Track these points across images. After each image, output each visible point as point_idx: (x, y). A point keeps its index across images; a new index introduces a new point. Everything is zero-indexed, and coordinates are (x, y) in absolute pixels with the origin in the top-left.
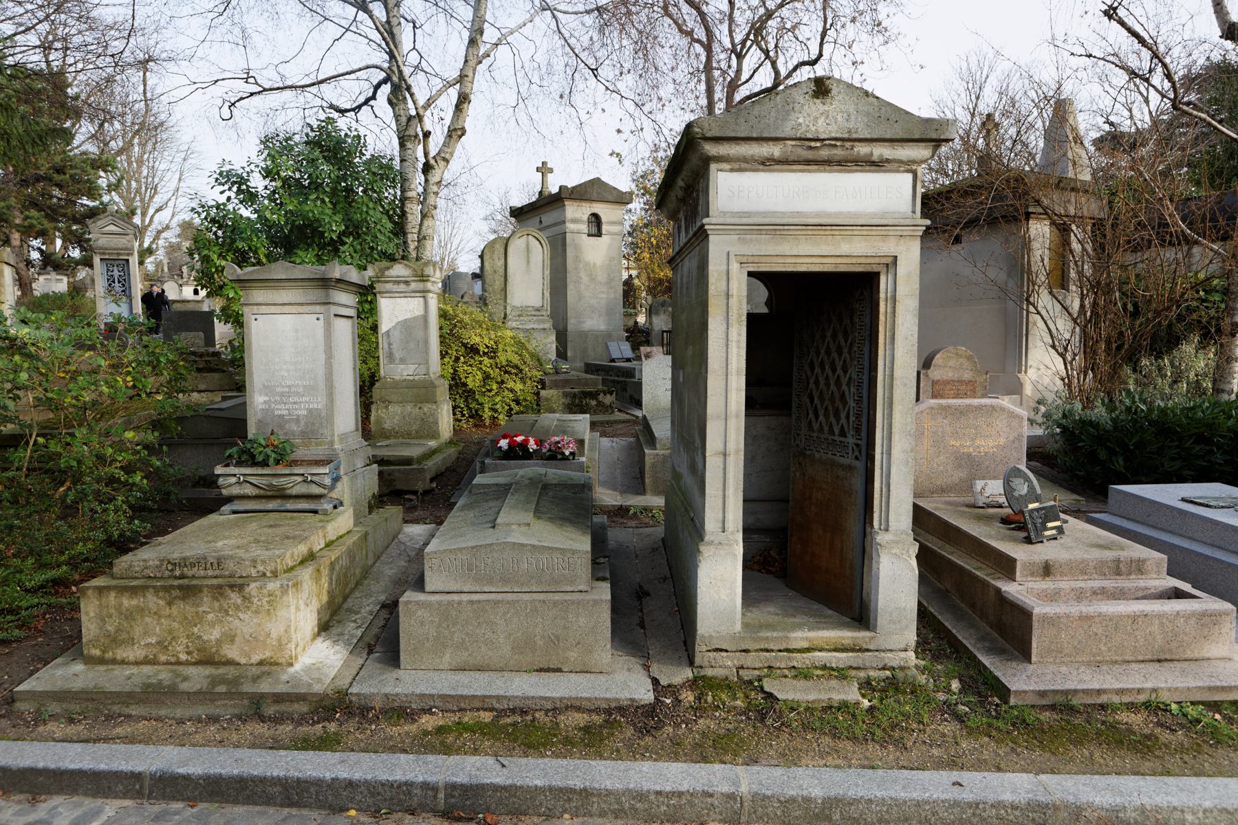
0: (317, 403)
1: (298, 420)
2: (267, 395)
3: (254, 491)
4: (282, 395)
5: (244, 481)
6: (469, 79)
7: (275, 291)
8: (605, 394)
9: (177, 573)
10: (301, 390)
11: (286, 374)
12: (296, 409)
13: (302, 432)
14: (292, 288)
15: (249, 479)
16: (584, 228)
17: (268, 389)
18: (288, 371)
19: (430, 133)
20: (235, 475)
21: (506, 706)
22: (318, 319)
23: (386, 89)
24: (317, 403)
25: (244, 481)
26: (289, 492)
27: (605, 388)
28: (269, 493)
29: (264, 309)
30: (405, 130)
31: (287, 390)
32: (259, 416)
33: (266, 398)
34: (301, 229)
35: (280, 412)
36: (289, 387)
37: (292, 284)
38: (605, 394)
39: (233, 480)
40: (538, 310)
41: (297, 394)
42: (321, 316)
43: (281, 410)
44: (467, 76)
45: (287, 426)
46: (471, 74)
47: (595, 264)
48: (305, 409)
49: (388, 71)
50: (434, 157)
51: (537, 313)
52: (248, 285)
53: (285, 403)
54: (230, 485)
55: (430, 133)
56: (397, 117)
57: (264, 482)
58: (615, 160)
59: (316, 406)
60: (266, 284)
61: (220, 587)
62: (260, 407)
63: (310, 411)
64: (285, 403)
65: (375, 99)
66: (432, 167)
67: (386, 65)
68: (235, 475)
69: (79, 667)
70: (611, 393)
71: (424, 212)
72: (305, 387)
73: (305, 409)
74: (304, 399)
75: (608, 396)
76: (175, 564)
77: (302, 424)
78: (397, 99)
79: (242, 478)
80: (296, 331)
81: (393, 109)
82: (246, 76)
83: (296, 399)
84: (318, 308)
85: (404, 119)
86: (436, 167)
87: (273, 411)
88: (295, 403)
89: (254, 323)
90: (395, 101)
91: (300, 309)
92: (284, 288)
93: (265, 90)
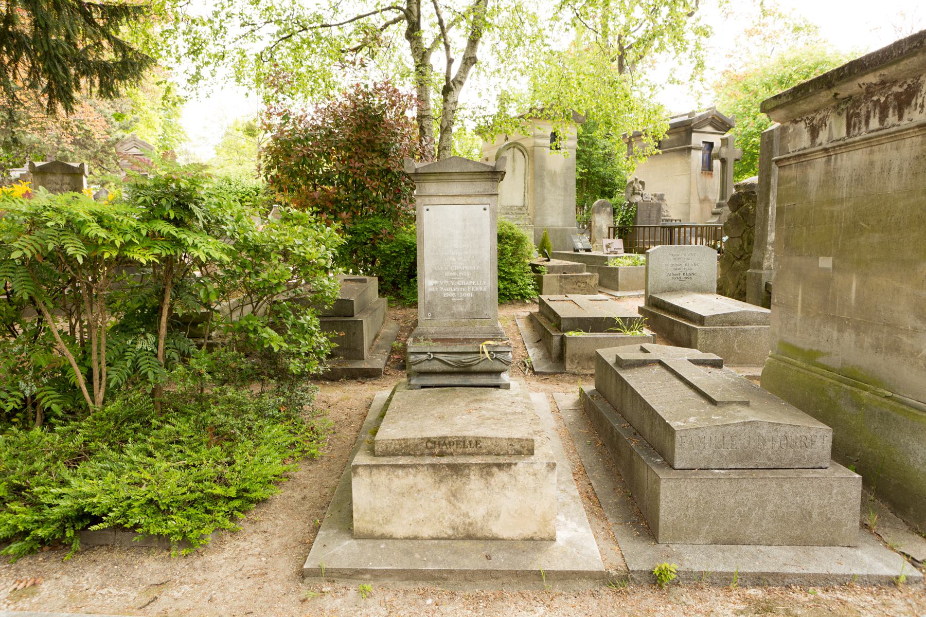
0: (483, 286)
1: (464, 301)
3: (445, 368)
4: (450, 278)
5: (434, 358)
9: (437, 451)
11: (454, 260)
12: (463, 292)
14: (463, 181)
15: (438, 356)
16: (547, 142)
17: (436, 273)
19: (453, 60)
20: (426, 353)
21: (735, 570)
22: (485, 209)
25: (434, 358)
26: (474, 368)
28: (456, 369)
29: (435, 200)
31: (455, 274)
32: (429, 298)
35: (448, 295)
36: (457, 271)
39: (424, 357)
40: (520, 209)
41: (465, 277)
42: (487, 207)
43: (449, 293)
45: (454, 308)
47: (555, 172)
48: (471, 291)
50: (453, 81)
51: (519, 211)
52: (424, 178)
53: (453, 287)
54: (421, 362)
55: (453, 60)
57: (453, 359)
58: (690, 77)
59: (481, 289)
61: (489, 465)
62: (430, 290)
63: (475, 293)
66: (451, 90)
67: (405, 7)
68: (426, 353)
69: (348, 543)
71: (444, 127)
72: (471, 271)
73: (471, 291)
74: (470, 282)
76: (435, 442)
79: (432, 356)
80: (464, 220)
83: (463, 282)
84: (485, 200)
86: (454, 89)
88: (461, 286)
89: (426, 213)
91: (470, 200)
92: (453, 181)
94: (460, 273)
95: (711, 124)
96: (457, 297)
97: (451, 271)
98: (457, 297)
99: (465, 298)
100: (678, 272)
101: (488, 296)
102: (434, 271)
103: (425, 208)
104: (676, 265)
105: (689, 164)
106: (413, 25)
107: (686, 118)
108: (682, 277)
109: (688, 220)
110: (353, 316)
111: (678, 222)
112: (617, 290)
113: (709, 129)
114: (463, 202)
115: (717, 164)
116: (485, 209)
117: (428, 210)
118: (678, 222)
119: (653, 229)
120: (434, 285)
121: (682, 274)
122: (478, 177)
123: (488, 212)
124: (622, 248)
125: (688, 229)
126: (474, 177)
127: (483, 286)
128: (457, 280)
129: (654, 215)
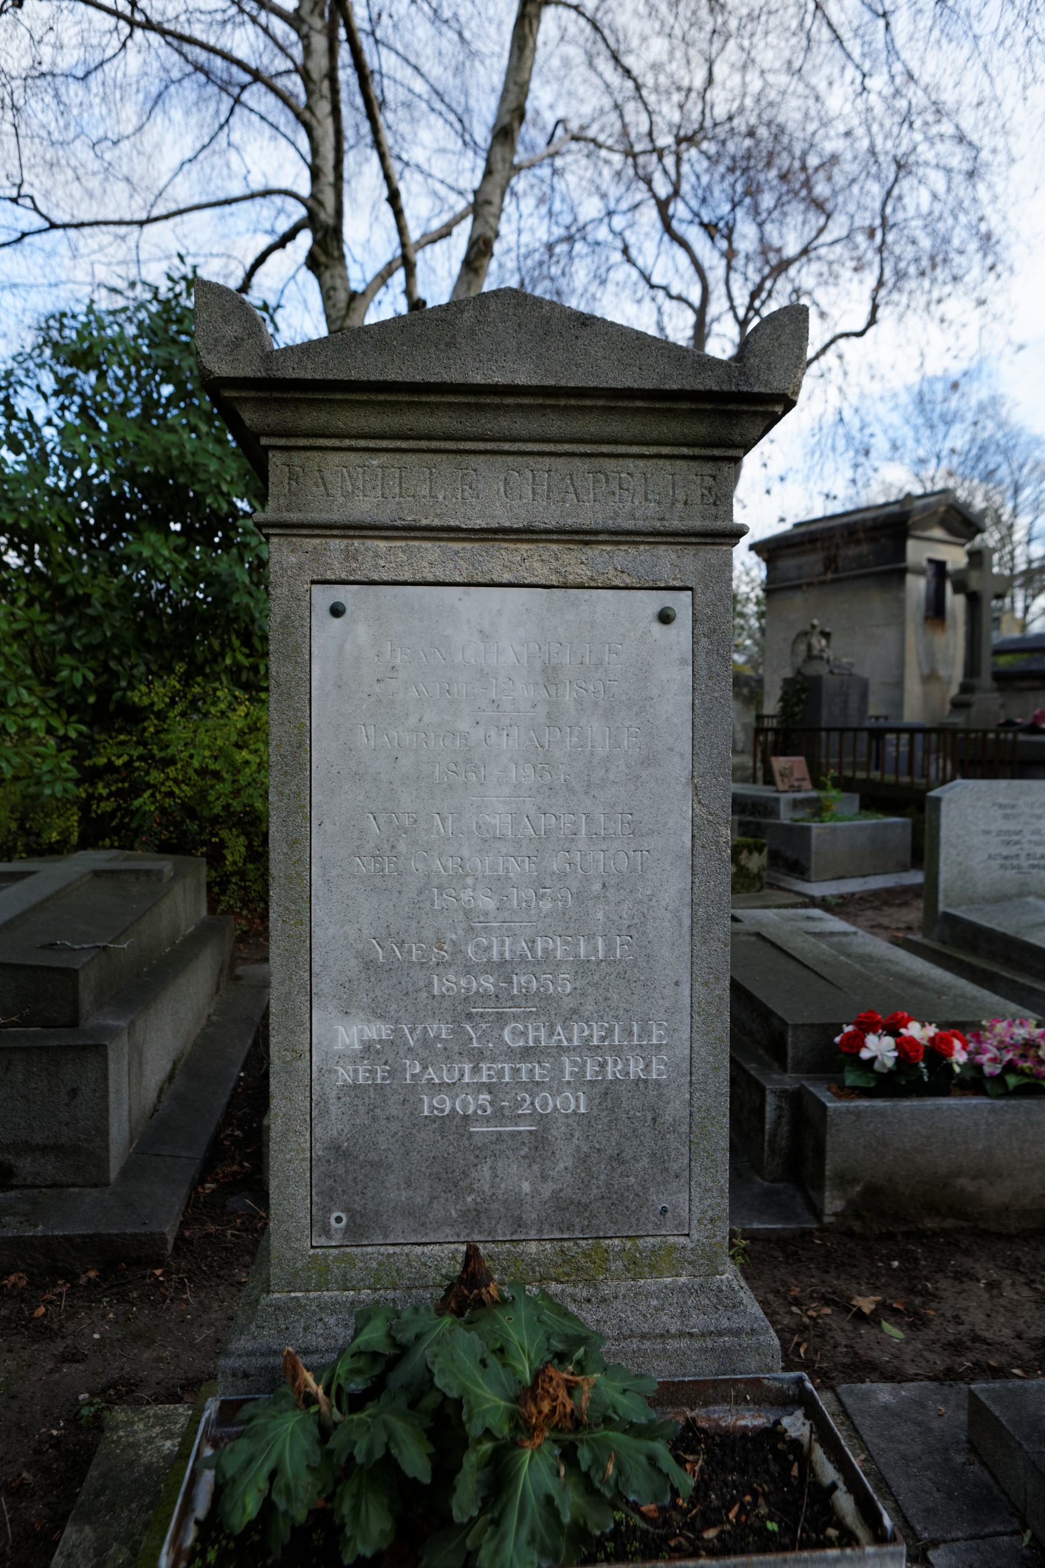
2: (380, 1015)
6: (493, 209)
7: (445, 465)
8: (750, 852)
10: (565, 985)
11: (489, 904)
13: (560, 1203)
18: (499, 884)
22: (665, 617)
23: (305, 240)
24: (646, 1052)
27: (750, 840)
30: (346, 316)
31: (488, 983)
33: (377, 1031)
34: (152, 485)
35: (446, 1104)
36: (503, 968)
37: (556, 425)
38: (750, 852)
42: (681, 603)
44: (489, 203)
46: (496, 200)
48: (579, 1082)
49: (310, 203)
52: (310, 419)
53: (477, 1057)
56: (327, 294)
59: (636, 1068)
60: (409, 420)
62: (344, 1075)
64: (477, 1057)
65: (246, 293)
70: (760, 850)
72: (582, 968)
74: (578, 1032)
75: (756, 855)
77: (565, 1161)
78: (327, 254)
81: (319, 277)
82: (14, 193)
83: (536, 1034)
85: (342, 297)
87: (410, 1095)
88: (526, 1053)
90: (323, 259)
93: (53, 226)
94: (519, 980)
95: (944, 524)
96: (499, 1115)
97: (468, 969)
98: (499, 1115)
99: (542, 1120)
100: (1014, 850)
101: (675, 1108)
102: (369, 965)
103: (323, 597)
104: (1008, 833)
105: (901, 603)
106: (325, 235)
107: (896, 508)
108: (1025, 863)
109: (900, 716)
110: (74, 1023)
111: (882, 721)
112: (808, 881)
113: (938, 533)
114: (542, 573)
115: (955, 603)
116: (665, 617)
117: (337, 611)
118: (882, 721)
119: (851, 734)
120: (368, 1048)
121: (1023, 855)
122: (633, 427)
123: (681, 632)
124: (807, 776)
125: (905, 737)
126: (615, 427)
127: (646, 1052)
128: (501, 1019)
129: (853, 704)
